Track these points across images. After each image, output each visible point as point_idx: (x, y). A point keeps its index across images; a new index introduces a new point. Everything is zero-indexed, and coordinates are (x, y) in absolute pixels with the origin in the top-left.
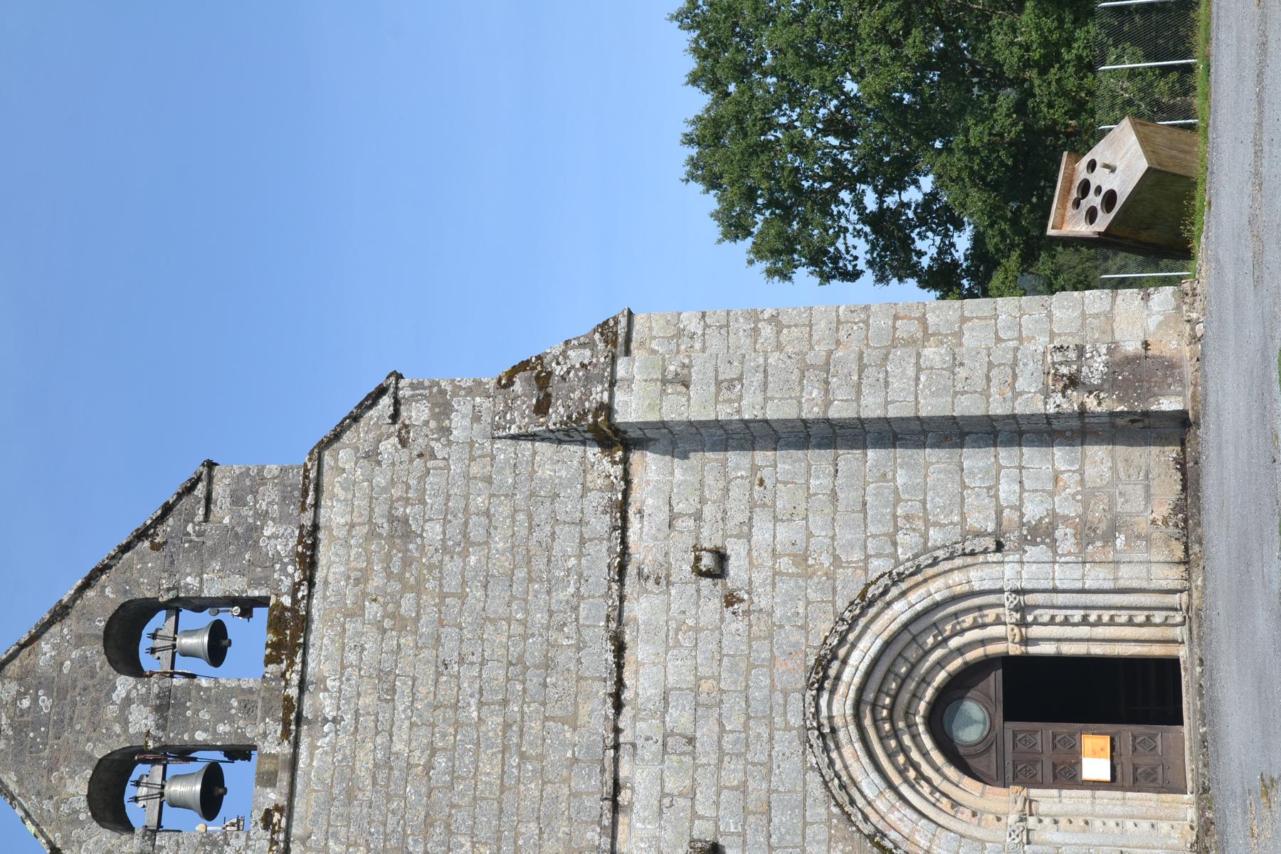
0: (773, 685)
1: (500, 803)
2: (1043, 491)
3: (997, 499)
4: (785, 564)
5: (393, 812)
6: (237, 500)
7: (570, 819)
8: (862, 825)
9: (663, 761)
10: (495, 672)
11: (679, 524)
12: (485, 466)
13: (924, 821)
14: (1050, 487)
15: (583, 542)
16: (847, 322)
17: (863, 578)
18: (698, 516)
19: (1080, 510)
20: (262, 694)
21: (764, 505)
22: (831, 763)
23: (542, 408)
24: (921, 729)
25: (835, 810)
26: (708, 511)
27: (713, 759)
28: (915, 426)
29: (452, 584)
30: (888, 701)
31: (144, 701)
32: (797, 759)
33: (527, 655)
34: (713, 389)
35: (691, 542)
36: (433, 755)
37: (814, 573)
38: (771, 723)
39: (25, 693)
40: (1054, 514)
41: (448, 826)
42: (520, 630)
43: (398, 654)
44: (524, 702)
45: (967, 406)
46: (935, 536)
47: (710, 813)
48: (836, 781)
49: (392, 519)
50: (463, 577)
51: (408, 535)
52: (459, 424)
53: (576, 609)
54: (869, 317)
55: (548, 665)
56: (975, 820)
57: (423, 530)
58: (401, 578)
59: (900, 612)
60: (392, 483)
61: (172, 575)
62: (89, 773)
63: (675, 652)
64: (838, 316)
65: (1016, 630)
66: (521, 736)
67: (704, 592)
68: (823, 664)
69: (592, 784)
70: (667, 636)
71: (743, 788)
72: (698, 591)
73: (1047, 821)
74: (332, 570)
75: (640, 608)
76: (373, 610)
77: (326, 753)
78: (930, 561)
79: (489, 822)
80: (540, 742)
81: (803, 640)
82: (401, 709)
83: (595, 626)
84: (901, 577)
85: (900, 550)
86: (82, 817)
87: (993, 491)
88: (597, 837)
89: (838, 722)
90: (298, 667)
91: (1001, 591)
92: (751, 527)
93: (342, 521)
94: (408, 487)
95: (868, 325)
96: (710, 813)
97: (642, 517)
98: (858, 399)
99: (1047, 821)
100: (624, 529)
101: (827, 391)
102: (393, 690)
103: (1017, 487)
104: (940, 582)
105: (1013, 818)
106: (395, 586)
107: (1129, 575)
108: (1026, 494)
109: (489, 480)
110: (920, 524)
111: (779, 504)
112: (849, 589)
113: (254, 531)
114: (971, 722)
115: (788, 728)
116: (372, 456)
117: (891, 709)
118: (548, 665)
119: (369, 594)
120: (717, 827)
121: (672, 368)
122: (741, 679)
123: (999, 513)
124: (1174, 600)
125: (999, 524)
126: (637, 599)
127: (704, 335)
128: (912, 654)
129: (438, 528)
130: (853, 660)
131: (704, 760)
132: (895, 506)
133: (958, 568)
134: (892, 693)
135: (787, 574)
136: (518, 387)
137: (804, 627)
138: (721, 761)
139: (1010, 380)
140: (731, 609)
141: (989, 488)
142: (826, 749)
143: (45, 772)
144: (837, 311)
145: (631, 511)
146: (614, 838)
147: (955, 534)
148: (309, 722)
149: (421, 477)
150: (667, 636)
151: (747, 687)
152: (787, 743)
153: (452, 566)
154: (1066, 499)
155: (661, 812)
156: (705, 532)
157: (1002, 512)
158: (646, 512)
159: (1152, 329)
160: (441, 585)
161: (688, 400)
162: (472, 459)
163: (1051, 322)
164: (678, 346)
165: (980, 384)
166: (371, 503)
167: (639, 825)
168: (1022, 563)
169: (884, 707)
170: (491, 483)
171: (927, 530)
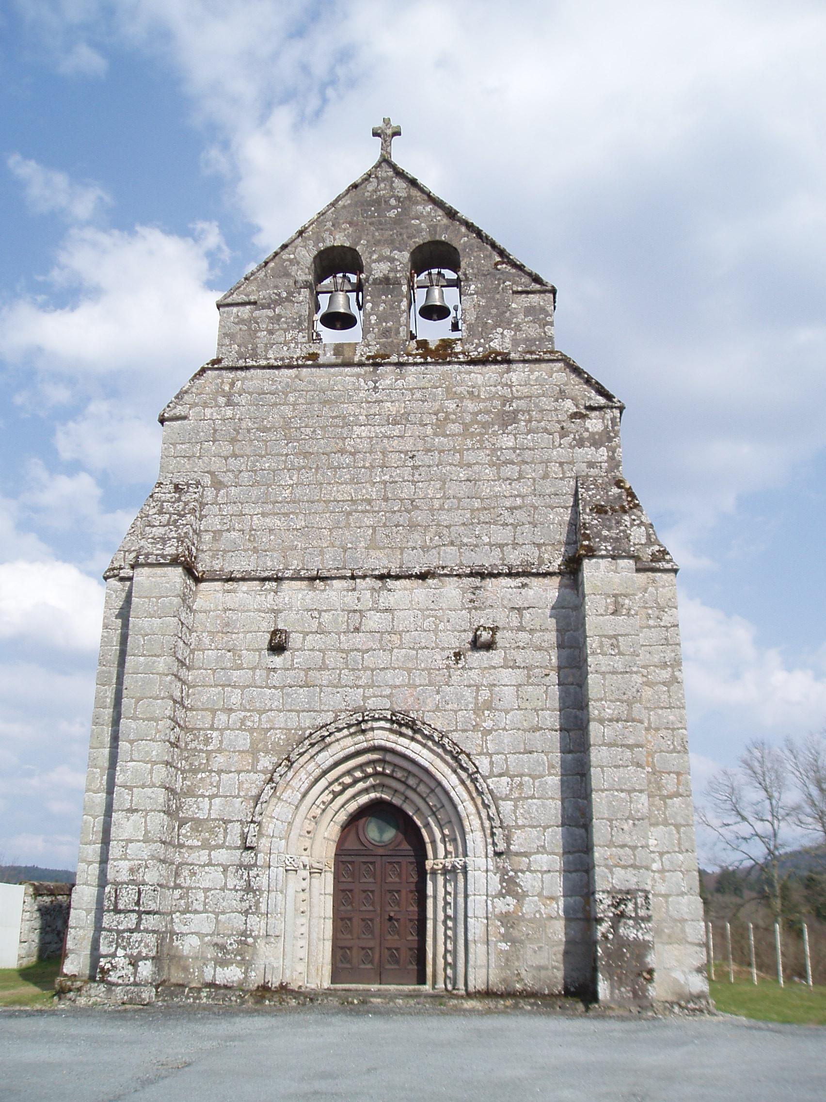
0: (396, 687)
1: (318, 501)
2: (543, 889)
3: (535, 853)
4: (485, 694)
5: (314, 431)
6: (529, 311)
7: (306, 548)
8: (296, 752)
9: (343, 610)
10: (407, 491)
11: (514, 615)
12: (556, 474)
13: (299, 796)
14: (545, 893)
15: (501, 546)
17: (475, 752)
18: (521, 629)
20: (395, 341)
22: (339, 730)
23: (600, 510)
24: (373, 795)
25: (308, 733)
26: (524, 636)
27: (345, 646)
28: (588, 792)
29: (470, 457)
30: (388, 771)
31: (394, 270)
32: (343, 706)
33: (419, 512)
34: (611, 633)
35: (500, 625)
36: (351, 454)
37: (478, 716)
39: (399, 201)
40: (525, 895)
42: (437, 506)
43: (420, 424)
44: (386, 512)
45: (600, 830)
46: (506, 806)
47: (307, 645)
48: (327, 734)
49: (516, 412)
50: (474, 464)
51: (504, 425)
52: (588, 452)
53: (452, 543)
54: (679, 752)
55: (413, 526)
56: (304, 833)
57: (508, 434)
58: (475, 421)
59: (450, 780)
60: (541, 411)
61: (475, 275)
62: (347, 244)
63: (420, 617)
64: (678, 729)
65: (441, 866)
66: (362, 512)
67: (464, 635)
68: (412, 725)
69: (328, 563)
70: (432, 610)
71: (324, 667)
72: (465, 631)
73: (305, 884)
74: (479, 376)
75: (452, 591)
76: (451, 405)
77: (354, 384)
78: (486, 802)
79: (306, 494)
80: (357, 525)
81: (428, 708)
82: (383, 430)
83: (439, 559)
84: (474, 781)
86: (321, 245)
88: (293, 567)
89: (370, 735)
90: (411, 360)
91: (465, 855)
93: (514, 380)
95: (671, 752)
96: (307, 645)
97: (519, 587)
98: (604, 744)
99: (305, 884)
100: (510, 575)
101: (610, 720)
102: (395, 423)
103: (545, 868)
104: (471, 809)
105: (306, 860)
106: (468, 418)
107: (478, 951)
108: (540, 875)
109: (545, 476)
110: (516, 795)
112: (470, 743)
113: (507, 325)
114: (381, 832)
116: (562, 395)
117: (382, 774)
118: (413, 526)
119: (462, 402)
120: (297, 650)
121: (627, 601)
122: (400, 664)
123: (526, 854)
124: (461, 985)
125: (517, 854)
126: (458, 587)
127: (660, 626)
128: (422, 788)
129: (511, 444)
130: (413, 745)
132: (530, 775)
133: (482, 824)
134: (395, 775)
135: (477, 695)
136: (615, 490)
137: (437, 709)
138: (343, 651)
140: (452, 655)
141: (543, 847)
142: (349, 726)
143: (349, 219)
144: (682, 728)
145: (523, 580)
146: (292, 579)
147: (509, 822)
148: (374, 372)
149: (547, 429)
150: (432, 610)
152: (355, 697)
153: (482, 456)
154: (536, 906)
155: (308, 610)
156: (508, 634)
157: (526, 856)
158: (523, 591)
160: (468, 449)
162: (561, 464)
163: (678, 895)
164: (651, 608)
165: (619, 839)
166: (528, 397)
167: (300, 596)
168: (487, 871)
169: (384, 768)
170: (543, 478)
171: (511, 800)
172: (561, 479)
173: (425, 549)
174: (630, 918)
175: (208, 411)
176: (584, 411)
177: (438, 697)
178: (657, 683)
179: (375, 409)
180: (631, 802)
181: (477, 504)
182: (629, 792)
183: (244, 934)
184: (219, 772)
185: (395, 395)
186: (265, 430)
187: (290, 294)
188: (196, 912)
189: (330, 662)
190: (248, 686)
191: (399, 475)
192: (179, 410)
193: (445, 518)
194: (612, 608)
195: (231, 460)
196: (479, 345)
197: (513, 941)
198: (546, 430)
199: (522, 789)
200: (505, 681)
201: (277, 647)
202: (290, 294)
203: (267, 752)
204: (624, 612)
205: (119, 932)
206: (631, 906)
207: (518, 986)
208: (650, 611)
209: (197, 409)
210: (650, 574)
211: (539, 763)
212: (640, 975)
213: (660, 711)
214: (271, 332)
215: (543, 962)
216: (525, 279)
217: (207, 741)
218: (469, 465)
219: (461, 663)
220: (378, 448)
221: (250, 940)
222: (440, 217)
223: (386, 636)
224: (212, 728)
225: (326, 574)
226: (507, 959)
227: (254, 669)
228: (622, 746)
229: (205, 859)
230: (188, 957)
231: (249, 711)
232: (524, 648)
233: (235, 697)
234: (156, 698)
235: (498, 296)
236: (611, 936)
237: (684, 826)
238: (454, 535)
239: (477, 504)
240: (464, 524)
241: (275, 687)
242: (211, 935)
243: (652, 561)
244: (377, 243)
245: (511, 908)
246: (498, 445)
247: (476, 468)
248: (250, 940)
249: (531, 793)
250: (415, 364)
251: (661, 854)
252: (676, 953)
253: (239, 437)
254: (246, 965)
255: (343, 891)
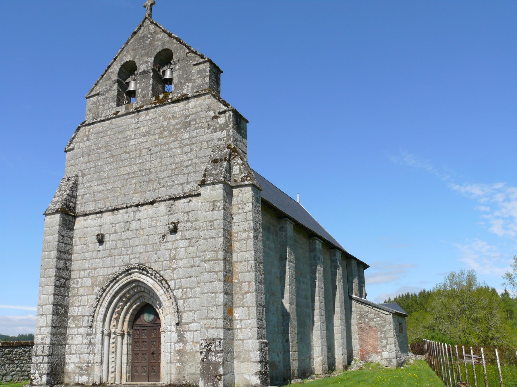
3: (191, 323)
10: (147, 166)
11: (186, 215)
14: (195, 341)
15: (182, 184)
16: (248, 264)
18: (188, 221)
19: (188, 351)
21: (190, 243)
26: (189, 224)
29: (172, 146)
31: (147, 67)
34: (211, 219)
35: (180, 220)
38: (131, 254)
40: (187, 342)
41: (112, 162)
42: (159, 170)
53: (164, 186)
55: (150, 181)
62: (131, 60)
66: (132, 178)
71: (116, 248)
75: (162, 207)
85: (176, 291)
87: (194, 321)
92: (184, 239)
94: (199, 124)
95: (246, 272)
96: (111, 239)
98: (206, 272)
100: (184, 197)
101: (209, 261)
102: (145, 136)
103: (195, 329)
106: (171, 128)
109: (200, 149)
110: (184, 297)
111: (191, 248)
115: (130, 259)
116: (209, 109)
118: (150, 181)
121: (218, 204)
123: (187, 323)
125: (185, 324)
131: (123, 234)
132: (190, 288)
135: (170, 254)
137: (156, 261)
139: (211, 326)
141: (194, 320)
145: (190, 198)
151: (140, 245)
155: (111, 224)
158: (189, 204)
159: (245, 376)
161: (207, 212)
162: (207, 142)
163: (248, 339)
165: (210, 316)
171: (182, 299)
172: (207, 149)
173: (154, 190)
174: (213, 351)
175: (81, 144)
176: (217, 115)
177: (156, 256)
178: (241, 240)
179: (138, 131)
180: (216, 298)
181: (174, 166)
182: (216, 293)
183: (88, 362)
184: (81, 296)
185: (145, 123)
186: (99, 148)
187: (111, 87)
188: (73, 354)
189: (119, 245)
190: (91, 259)
191: (145, 159)
192: (72, 146)
193: (161, 175)
194: (212, 208)
195: (88, 164)
196: (178, 93)
197: (182, 362)
198: (202, 127)
199: (186, 294)
200: (181, 246)
201: (101, 240)
202: (111, 87)
203: (97, 286)
204: (217, 208)
205: (37, 364)
206: (213, 346)
207: (184, 382)
208: (239, 206)
209: (77, 144)
210: (240, 188)
211: (193, 282)
212: (216, 377)
213: (242, 253)
214: (104, 105)
215: (194, 371)
216: (198, 58)
217: (77, 283)
218: (171, 149)
219: (165, 240)
220: (138, 148)
221: (90, 365)
222: (166, 38)
223: (138, 231)
224: (79, 278)
225: (117, 207)
226: (180, 370)
227: (92, 251)
228: (213, 272)
229: (76, 332)
230: (70, 373)
231: (91, 269)
232: (189, 230)
233: (87, 264)
234: (50, 268)
235: (187, 69)
236: (205, 360)
237: (251, 307)
238: (165, 182)
239: (174, 166)
240: (168, 177)
241: (100, 258)
242: (78, 363)
243: (241, 181)
244: (142, 56)
245: (182, 348)
246: (183, 138)
247: (174, 150)
248: (90, 365)
249: (190, 296)
250: (153, 108)
251: (241, 320)
252: (246, 366)
253: (91, 154)
254: (89, 375)
255: (136, 342)
